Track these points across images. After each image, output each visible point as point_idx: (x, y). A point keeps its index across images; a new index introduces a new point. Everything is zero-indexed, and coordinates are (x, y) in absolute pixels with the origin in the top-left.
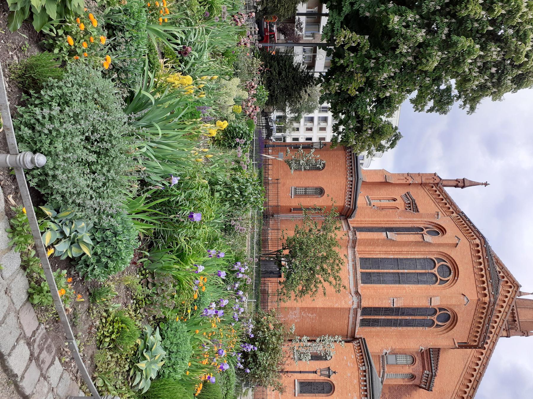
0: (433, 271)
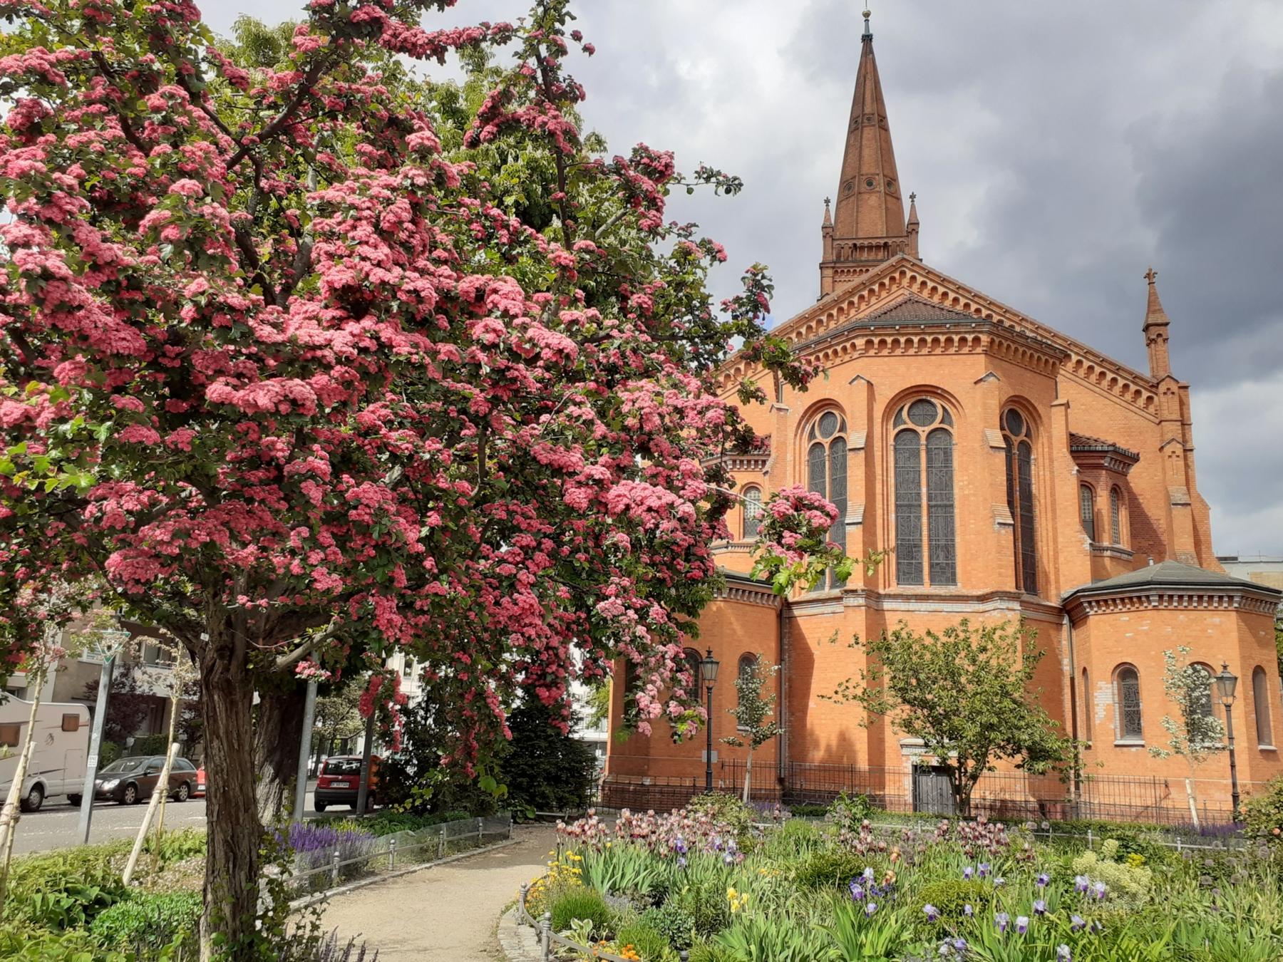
0: (923, 436)
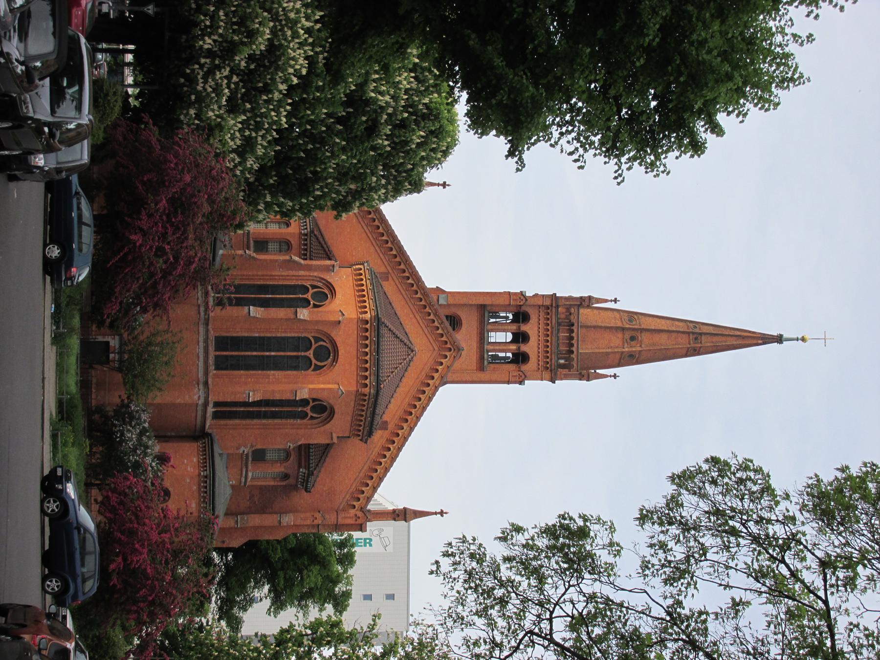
0: (307, 354)
